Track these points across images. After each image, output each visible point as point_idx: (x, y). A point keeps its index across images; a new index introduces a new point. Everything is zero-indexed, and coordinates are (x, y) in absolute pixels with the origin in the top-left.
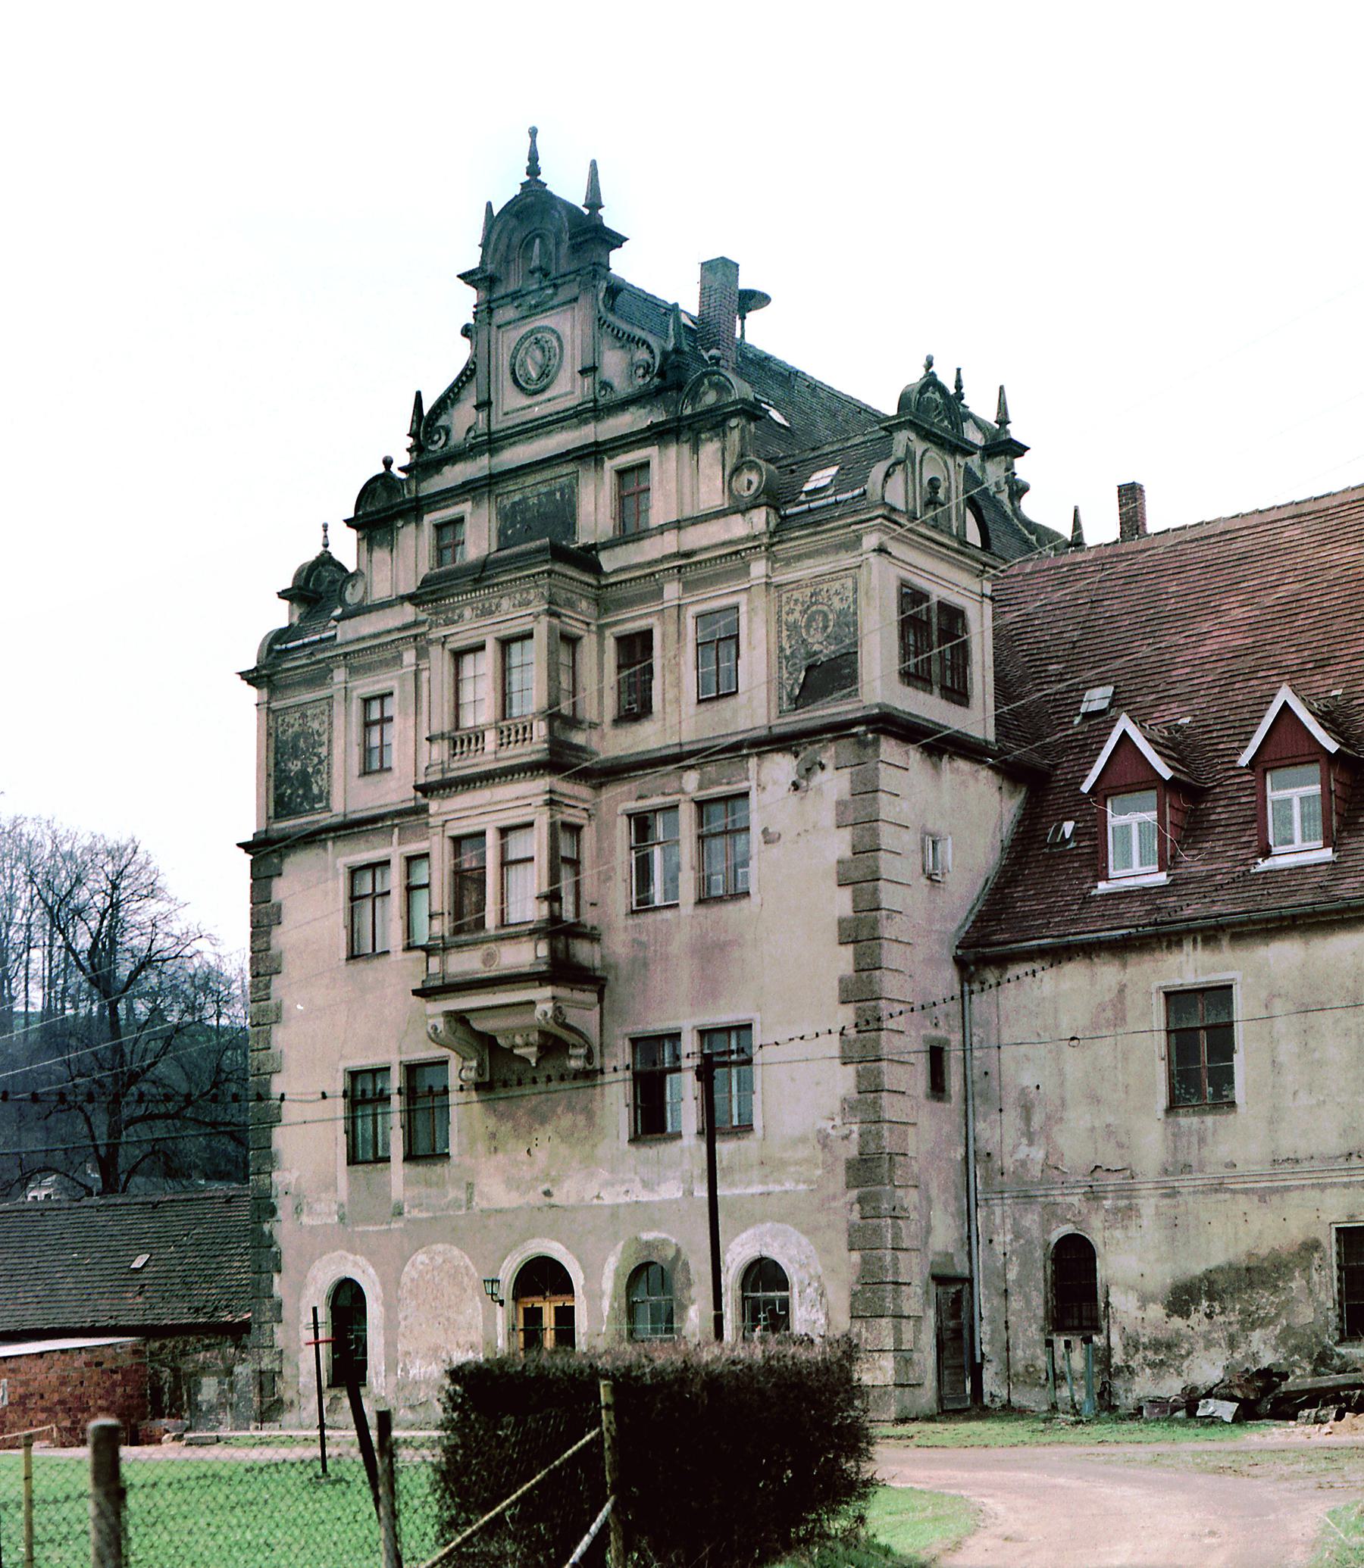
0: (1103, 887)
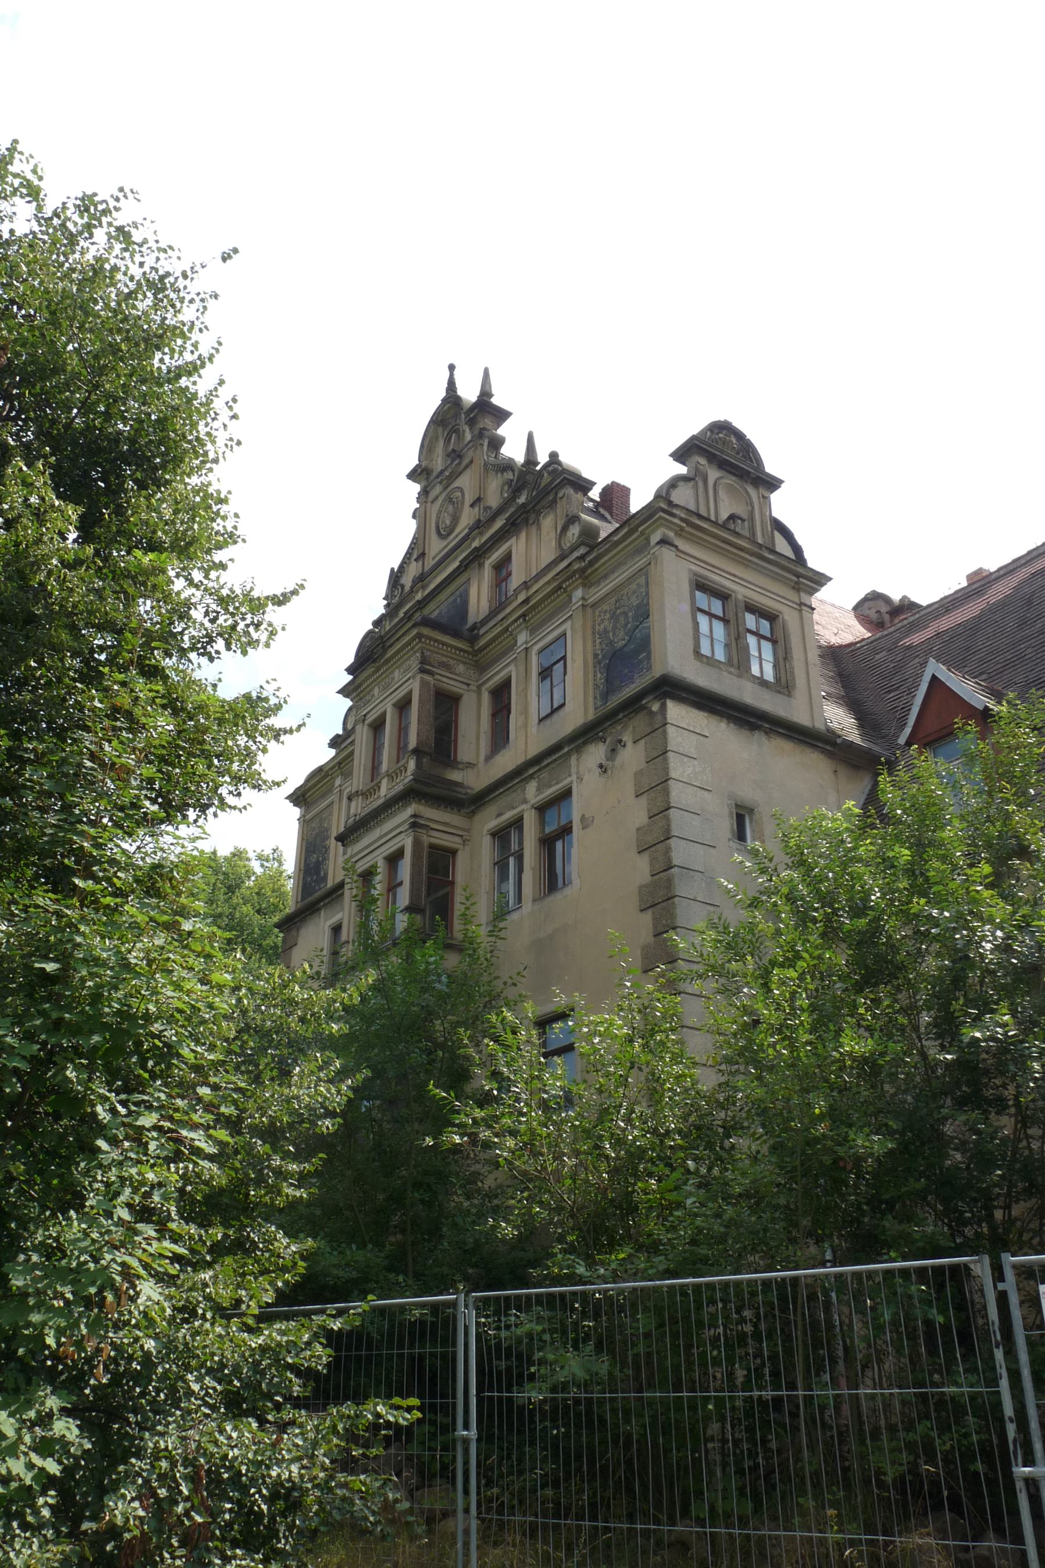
0: (538, 468)
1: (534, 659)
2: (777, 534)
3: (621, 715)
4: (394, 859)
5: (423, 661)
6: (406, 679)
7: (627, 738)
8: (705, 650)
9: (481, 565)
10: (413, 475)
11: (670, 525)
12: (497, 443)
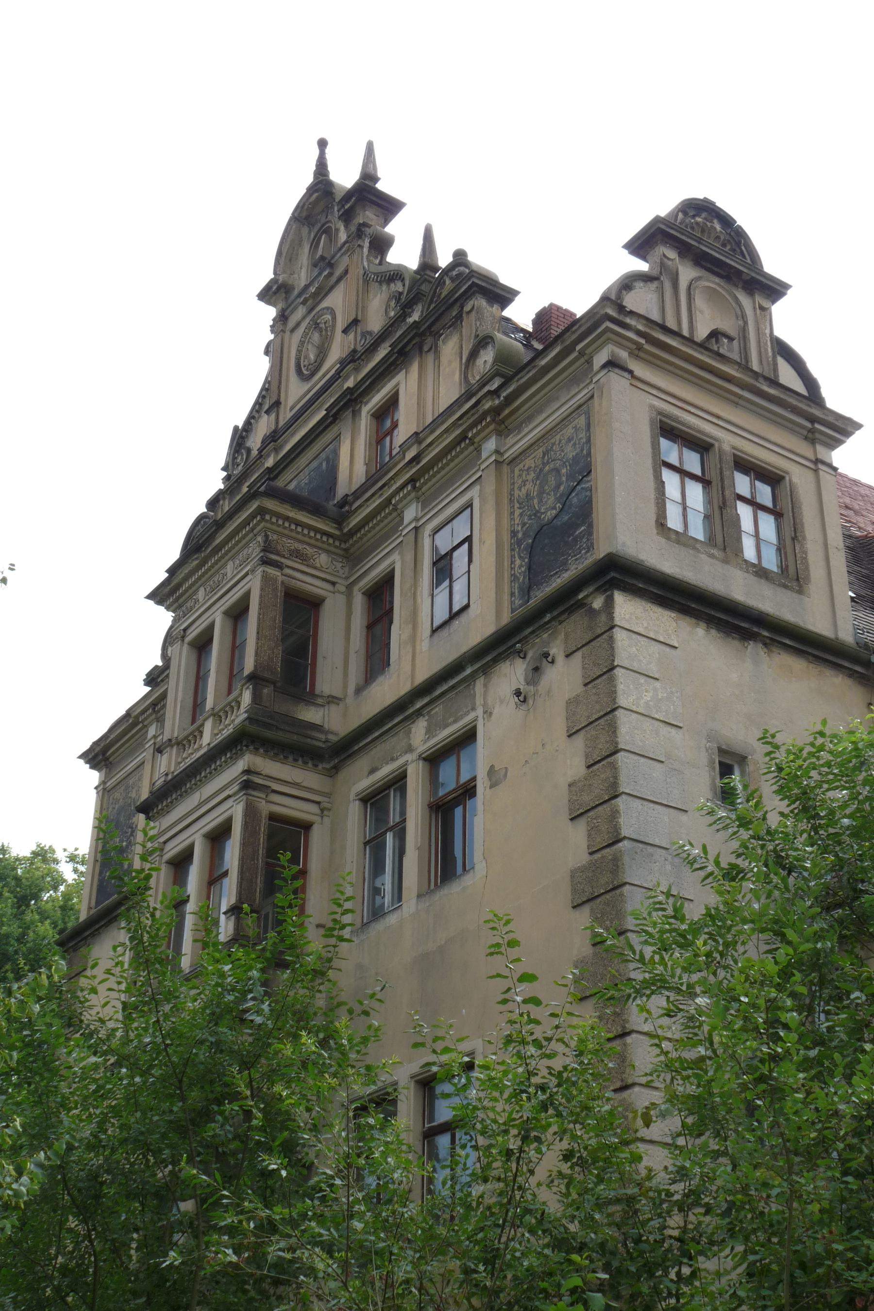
1: (427, 542)
2: (780, 361)
3: (548, 617)
4: (218, 837)
5: (267, 548)
6: (244, 576)
7: (556, 650)
8: (674, 521)
9: (356, 414)
10: (267, 295)
12: (382, 245)
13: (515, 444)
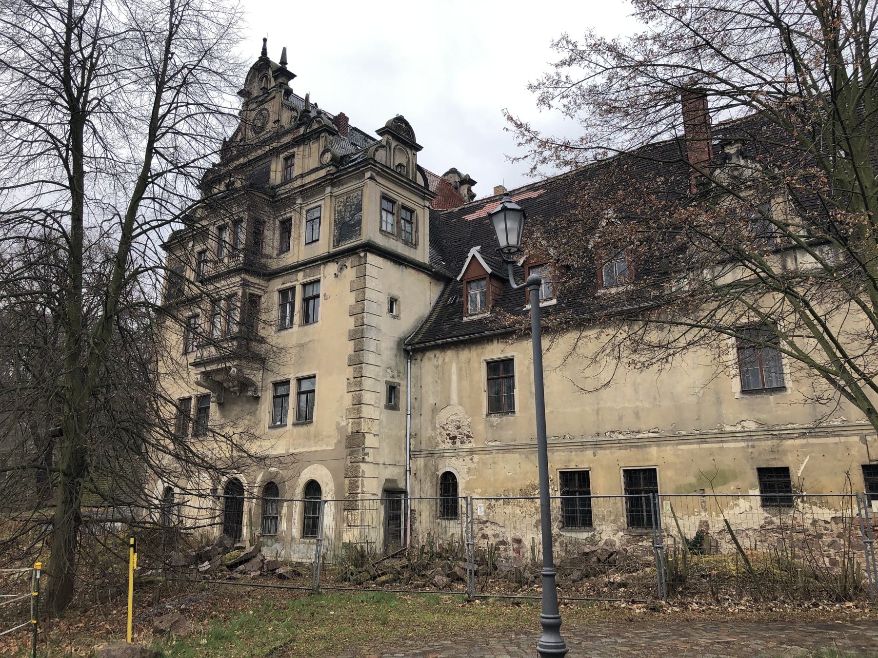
7: (348, 264)
8: (384, 228)
9: (278, 156)
11: (374, 170)
13: (338, 191)
